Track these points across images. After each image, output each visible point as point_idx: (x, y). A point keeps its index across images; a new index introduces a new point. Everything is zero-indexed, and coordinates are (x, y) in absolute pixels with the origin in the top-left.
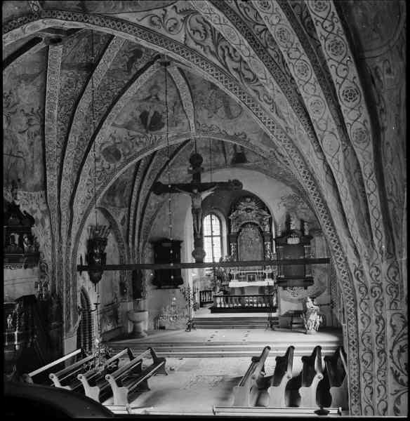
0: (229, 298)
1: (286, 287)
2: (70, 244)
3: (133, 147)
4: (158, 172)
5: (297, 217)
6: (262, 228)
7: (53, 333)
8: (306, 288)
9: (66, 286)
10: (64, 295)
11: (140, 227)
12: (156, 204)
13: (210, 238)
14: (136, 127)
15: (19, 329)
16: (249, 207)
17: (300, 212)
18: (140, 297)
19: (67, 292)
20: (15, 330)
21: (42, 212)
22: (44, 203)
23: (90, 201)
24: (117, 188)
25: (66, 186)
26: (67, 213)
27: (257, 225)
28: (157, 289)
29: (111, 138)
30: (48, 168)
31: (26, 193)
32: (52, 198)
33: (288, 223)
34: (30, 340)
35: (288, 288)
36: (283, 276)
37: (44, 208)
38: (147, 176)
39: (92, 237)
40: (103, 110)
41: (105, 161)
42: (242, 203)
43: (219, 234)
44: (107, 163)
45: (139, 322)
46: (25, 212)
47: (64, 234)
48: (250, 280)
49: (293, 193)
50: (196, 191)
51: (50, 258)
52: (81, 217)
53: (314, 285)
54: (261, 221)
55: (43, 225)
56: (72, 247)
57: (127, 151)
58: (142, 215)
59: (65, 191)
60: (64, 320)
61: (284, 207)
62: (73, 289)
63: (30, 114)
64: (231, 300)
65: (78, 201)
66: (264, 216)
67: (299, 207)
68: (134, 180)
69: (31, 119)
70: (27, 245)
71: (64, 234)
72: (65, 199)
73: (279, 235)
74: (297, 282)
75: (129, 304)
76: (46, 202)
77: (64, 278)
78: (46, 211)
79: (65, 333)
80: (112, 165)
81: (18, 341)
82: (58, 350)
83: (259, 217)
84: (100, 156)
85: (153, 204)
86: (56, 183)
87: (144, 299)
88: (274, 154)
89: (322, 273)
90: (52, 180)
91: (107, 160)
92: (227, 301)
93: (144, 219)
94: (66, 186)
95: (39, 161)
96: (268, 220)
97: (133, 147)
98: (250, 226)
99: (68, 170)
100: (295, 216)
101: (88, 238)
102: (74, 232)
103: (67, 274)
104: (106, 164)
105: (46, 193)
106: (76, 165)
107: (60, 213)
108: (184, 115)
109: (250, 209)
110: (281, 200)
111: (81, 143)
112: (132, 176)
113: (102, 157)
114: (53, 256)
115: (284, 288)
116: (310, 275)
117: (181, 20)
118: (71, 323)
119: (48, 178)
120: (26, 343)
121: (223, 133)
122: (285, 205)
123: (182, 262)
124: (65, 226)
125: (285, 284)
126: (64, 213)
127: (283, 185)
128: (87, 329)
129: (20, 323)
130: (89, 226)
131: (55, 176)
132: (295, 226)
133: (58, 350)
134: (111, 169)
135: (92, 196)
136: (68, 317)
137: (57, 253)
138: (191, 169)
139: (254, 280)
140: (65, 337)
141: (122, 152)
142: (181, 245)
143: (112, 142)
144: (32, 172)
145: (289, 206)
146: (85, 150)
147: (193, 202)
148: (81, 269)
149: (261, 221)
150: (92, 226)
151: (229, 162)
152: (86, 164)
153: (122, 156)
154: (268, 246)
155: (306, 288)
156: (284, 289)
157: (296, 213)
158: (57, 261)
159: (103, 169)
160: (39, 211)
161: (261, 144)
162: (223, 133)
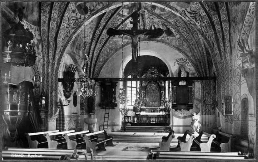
1: (177, 109)
2: (54, 64)
3: (96, 5)
4: (105, 40)
5: (185, 70)
6: (160, 84)
7: (43, 115)
8: (188, 111)
9: (51, 89)
10: (50, 95)
11: (93, 73)
12: (103, 60)
13: (131, 88)
17: (187, 68)
18: (92, 112)
19: (51, 93)
20: (18, 103)
22: (39, 35)
24: (81, 46)
25: (53, 25)
26: (53, 44)
28: (101, 109)
30: (42, 11)
31: (28, 23)
32: (44, 32)
33: (180, 73)
35: (178, 110)
36: (175, 103)
38: (99, 42)
39: (66, 71)
41: (78, 13)
42: (150, 69)
43: (135, 86)
44: (80, 15)
45: (92, 124)
47: (51, 57)
48: (152, 112)
49: (184, 57)
51: (41, 71)
52: (62, 48)
53: (193, 109)
56: (56, 66)
57: (92, 8)
58: (95, 65)
59: (53, 28)
60: (49, 114)
61: (178, 65)
62: (55, 92)
65: (60, 37)
67: (186, 65)
68: (91, 43)
70: (28, 47)
71: (51, 57)
72: (52, 34)
74: (183, 107)
75: (85, 116)
76: (40, 35)
77: (50, 84)
78: (40, 40)
79: (49, 118)
80: (83, 16)
82: (45, 126)
84: (75, 10)
85: (101, 59)
86: (47, 22)
87: (94, 114)
88: (185, 12)
89: (198, 102)
90: (44, 20)
91: (79, 13)
93: (96, 68)
94: (53, 25)
95: (37, 5)
97: (96, 5)
100: (184, 70)
101: (64, 71)
102: (57, 57)
103: (52, 82)
104: (79, 15)
105: (40, 29)
106: (60, 13)
107: (49, 43)
109: (153, 73)
110: (175, 61)
112: (90, 40)
113: (77, 10)
114: (43, 70)
116: (191, 103)
118: (53, 113)
119: (42, 18)
122: (178, 64)
123: (123, 82)
124: (51, 52)
126: (51, 43)
127: (177, 52)
128: (61, 126)
130: (64, 64)
131: (46, 17)
132: (183, 75)
133: (45, 126)
134: (81, 19)
136: (52, 109)
137: (46, 68)
138: (132, 21)
139: (154, 112)
140: (49, 120)
141: (89, 8)
142: (117, 84)
144: (33, 11)
145: (180, 65)
148: (60, 80)
150: (66, 65)
152: (66, 12)
153: (89, 11)
154: (163, 93)
155: (188, 111)
157: (184, 68)
158: (45, 73)
159: (77, 19)
161: (177, 6)
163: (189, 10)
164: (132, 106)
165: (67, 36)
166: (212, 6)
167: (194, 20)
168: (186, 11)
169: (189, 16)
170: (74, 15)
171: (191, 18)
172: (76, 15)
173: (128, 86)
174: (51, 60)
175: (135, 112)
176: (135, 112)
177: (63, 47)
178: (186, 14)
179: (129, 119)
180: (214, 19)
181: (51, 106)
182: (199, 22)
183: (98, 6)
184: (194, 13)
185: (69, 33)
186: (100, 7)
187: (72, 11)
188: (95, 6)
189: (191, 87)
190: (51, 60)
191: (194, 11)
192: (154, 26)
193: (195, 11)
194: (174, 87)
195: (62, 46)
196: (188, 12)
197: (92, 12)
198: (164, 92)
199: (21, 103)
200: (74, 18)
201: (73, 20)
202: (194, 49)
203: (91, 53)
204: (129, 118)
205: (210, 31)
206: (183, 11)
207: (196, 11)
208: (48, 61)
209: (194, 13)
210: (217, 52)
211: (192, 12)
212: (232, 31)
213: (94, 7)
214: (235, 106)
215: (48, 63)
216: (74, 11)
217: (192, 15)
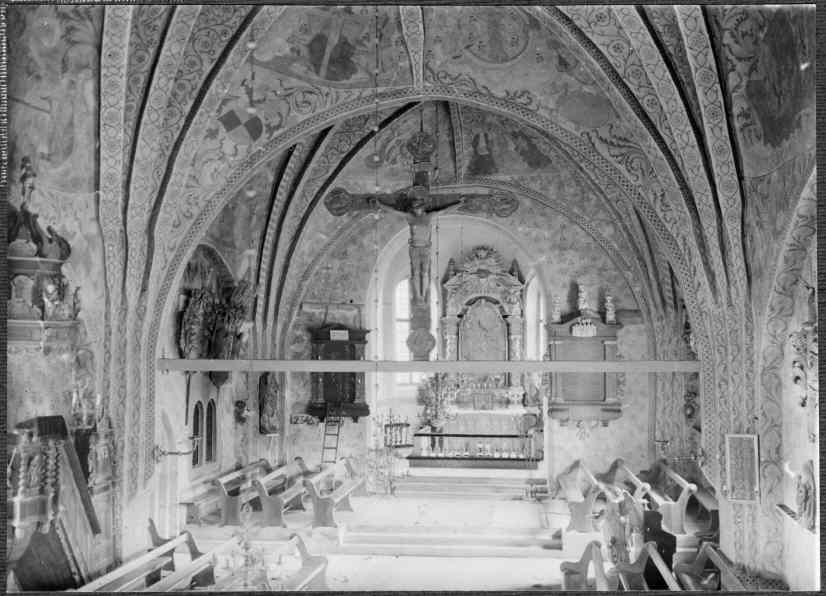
0: (437, 438)
14: (298, 68)
15: (24, 492)
16: (483, 267)
21: (87, 237)
23: (188, 224)
27: (497, 302)
29: (243, 89)
34: (50, 517)
37: (93, 229)
40: (230, 23)
46: (49, 230)
50: (419, 211)
54: (506, 293)
55: (88, 265)
57: (275, 121)
63: (72, 15)
64: (441, 443)
66: (511, 285)
69: (72, 28)
73: (557, 318)
81: (23, 517)
83: (502, 288)
88: (590, 139)
92: (433, 445)
96: (518, 293)
98: (483, 301)
99: (147, 151)
108: (402, 48)
109: (483, 271)
111: (181, 94)
113: (223, 129)
115: (563, 422)
117: (72, 431)
120: (39, 524)
121: (484, 91)
125: (564, 416)
129: (28, 478)
134: (239, 157)
135: (196, 211)
141: (263, 121)
142: (367, 336)
143: (246, 99)
146: (187, 109)
147: (412, 233)
149: (506, 293)
151: (463, 171)
153: (264, 128)
156: (561, 425)
160: (78, 235)
162: (484, 91)
163: (605, 134)
164: (411, 383)
165: (188, 214)
166: (683, 131)
167: (622, 168)
168: (593, 135)
169: (605, 154)
170: (212, 144)
171: (610, 159)
172: (222, 144)
173: (399, 316)
174: (132, 301)
175: (423, 407)
176: (423, 407)
177: (174, 253)
178: (593, 144)
179: (404, 435)
180: (690, 175)
181: (133, 459)
182: (639, 173)
183: (293, 113)
184: (621, 143)
185: (197, 204)
186: (301, 118)
187: (205, 133)
188: (284, 112)
189: (615, 343)
190: (132, 301)
191: (620, 139)
192: (486, 135)
193: (625, 140)
194: (557, 343)
195: (172, 250)
196: (601, 139)
197: (276, 133)
198: (520, 337)
199: (26, 497)
200: (212, 156)
201: (211, 160)
202: (624, 216)
203: (267, 248)
204: (401, 432)
205: (678, 210)
206: (585, 136)
207: (628, 136)
208: (122, 303)
209: (621, 143)
210: (704, 279)
211: (614, 140)
212: (751, 218)
213: (280, 115)
214: (739, 80)
215: (124, 309)
216: (212, 134)
217: (616, 151)
